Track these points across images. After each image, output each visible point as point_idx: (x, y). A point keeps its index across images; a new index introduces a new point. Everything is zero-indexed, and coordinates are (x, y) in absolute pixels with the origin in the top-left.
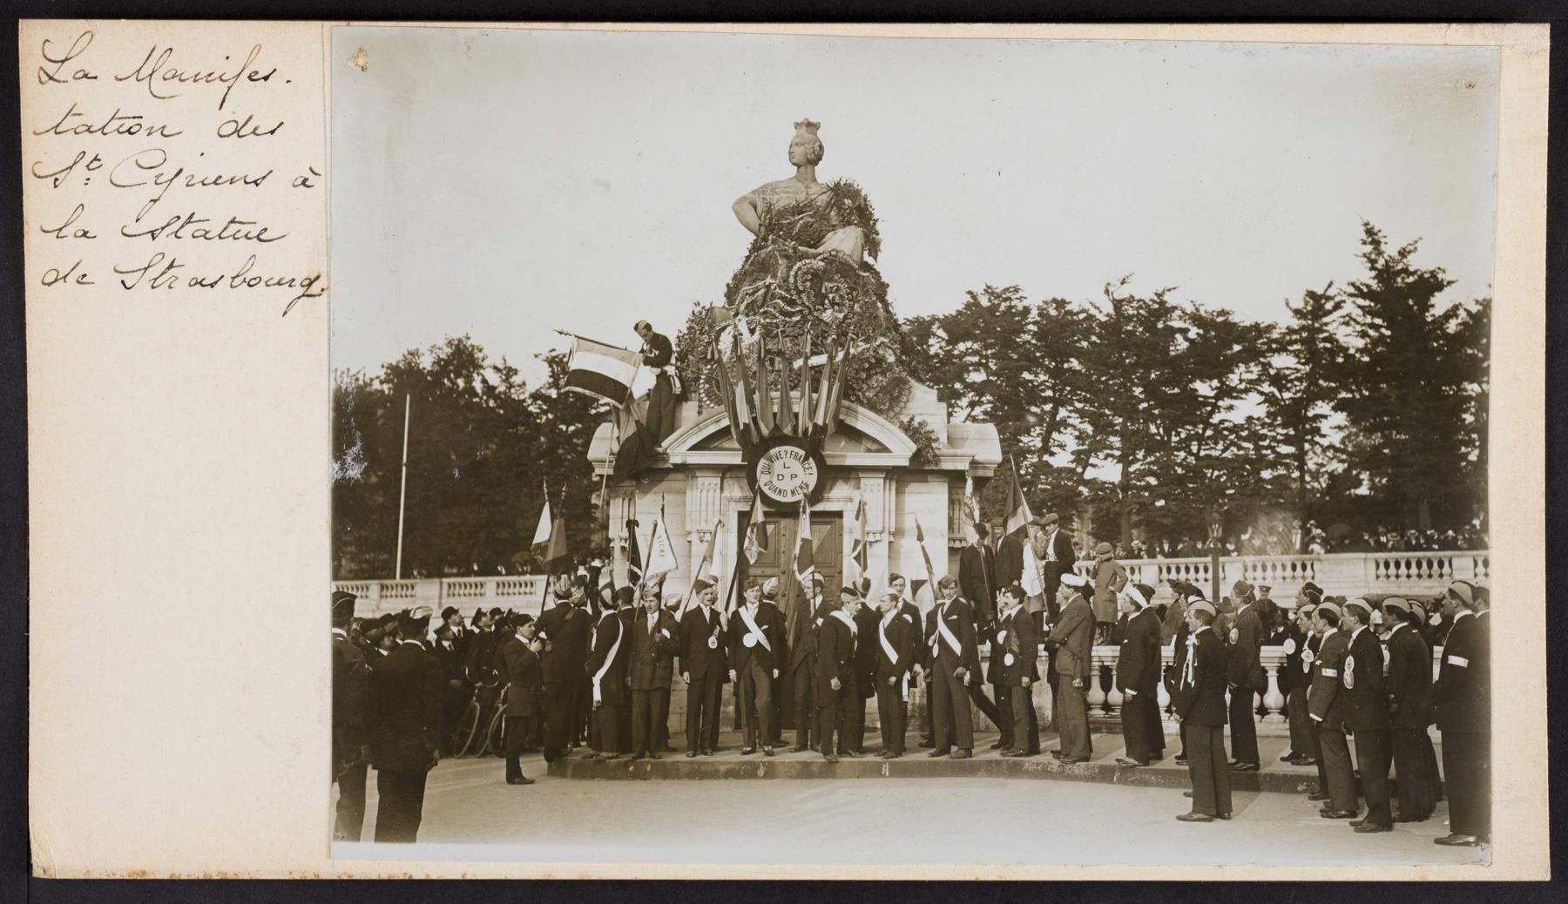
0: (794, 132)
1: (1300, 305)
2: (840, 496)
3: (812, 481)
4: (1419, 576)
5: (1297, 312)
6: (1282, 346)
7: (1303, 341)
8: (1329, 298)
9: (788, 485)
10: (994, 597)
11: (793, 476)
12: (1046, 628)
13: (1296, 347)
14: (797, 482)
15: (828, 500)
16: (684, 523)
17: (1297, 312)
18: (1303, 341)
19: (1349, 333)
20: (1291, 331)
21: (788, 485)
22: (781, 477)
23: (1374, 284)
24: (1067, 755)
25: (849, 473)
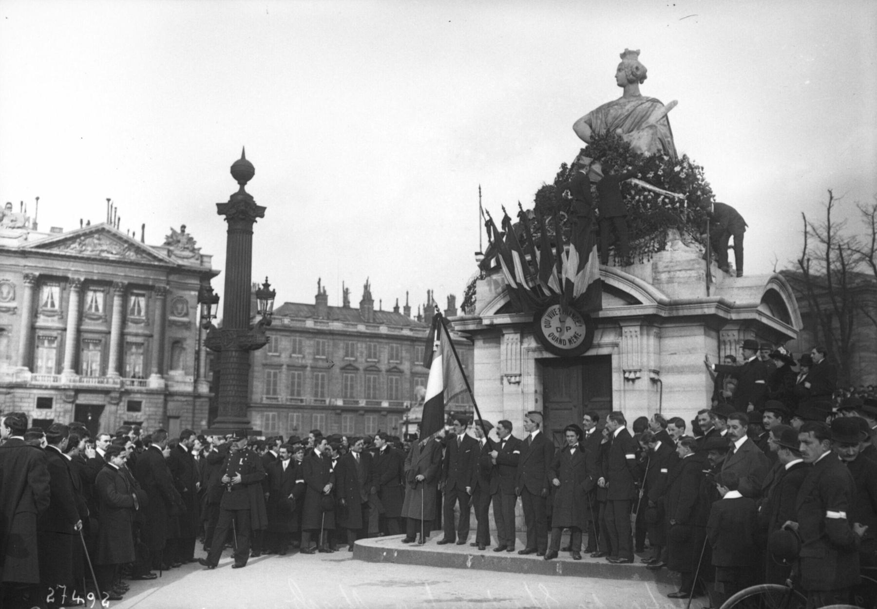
0: (620, 61)
11: (568, 328)
15: (599, 346)
21: (566, 336)
25: (616, 324)
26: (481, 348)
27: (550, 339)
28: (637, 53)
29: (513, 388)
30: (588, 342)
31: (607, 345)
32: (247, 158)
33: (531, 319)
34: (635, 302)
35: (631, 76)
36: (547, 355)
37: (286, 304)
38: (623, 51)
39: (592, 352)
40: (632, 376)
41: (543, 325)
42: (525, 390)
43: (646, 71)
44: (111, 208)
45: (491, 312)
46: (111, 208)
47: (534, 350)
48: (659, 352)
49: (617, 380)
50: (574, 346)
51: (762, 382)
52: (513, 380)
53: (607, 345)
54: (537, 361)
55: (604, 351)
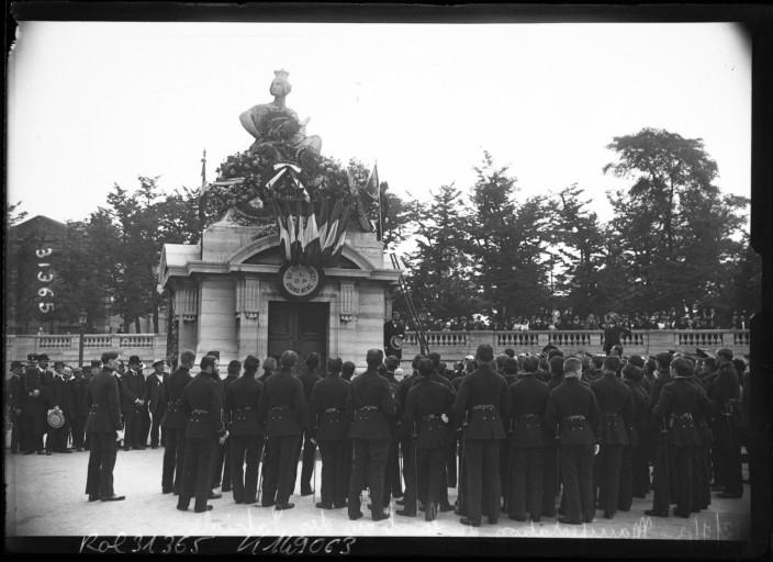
0: (274, 77)
1: (438, 193)
2: (327, 295)
3: (314, 284)
4: (521, 343)
5: (437, 198)
6: (428, 216)
7: (440, 213)
8: (453, 190)
9: (300, 286)
10: (151, 271)
11: (305, 281)
12: (557, 437)
13: (437, 216)
14: (306, 284)
15: (322, 295)
16: (235, 307)
17: (437, 198)
18: (440, 213)
19: (466, 208)
20: (434, 207)
21: (300, 286)
22: (297, 281)
23: (623, 151)
24: (152, 284)
25: (337, 282)
26: (207, 287)
27: (287, 288)
28: (287, 74)
29: (250, 323)
30: (316, 293)
31: (327, 296)
32: (290, 103)
33: (275, 271)
34: (354, 267)
35: (280, 91)
36: (279, 299)
37: (39, 217)
38: (279, 69)
39: (316, 300)
40: (347, 319)
41: (285, 276)
42: (261, 324)
43: (289, 90)
44: (308, 120)
45: (239, 262)
46: (308, 120)
47: (268, 295)
48: (361, 303)
49: (333, 321)
50: (305, 294)
51: (45, 436)
52: (251, 316)
53: (327, 296)
54: (270, 303)
55: (325, 300)
